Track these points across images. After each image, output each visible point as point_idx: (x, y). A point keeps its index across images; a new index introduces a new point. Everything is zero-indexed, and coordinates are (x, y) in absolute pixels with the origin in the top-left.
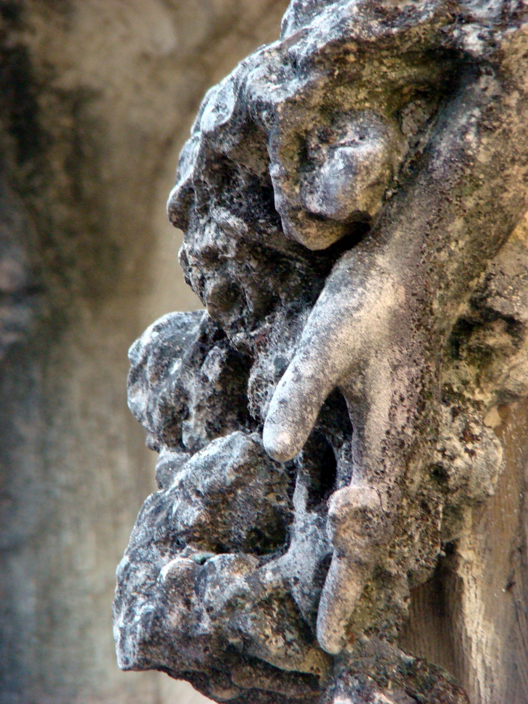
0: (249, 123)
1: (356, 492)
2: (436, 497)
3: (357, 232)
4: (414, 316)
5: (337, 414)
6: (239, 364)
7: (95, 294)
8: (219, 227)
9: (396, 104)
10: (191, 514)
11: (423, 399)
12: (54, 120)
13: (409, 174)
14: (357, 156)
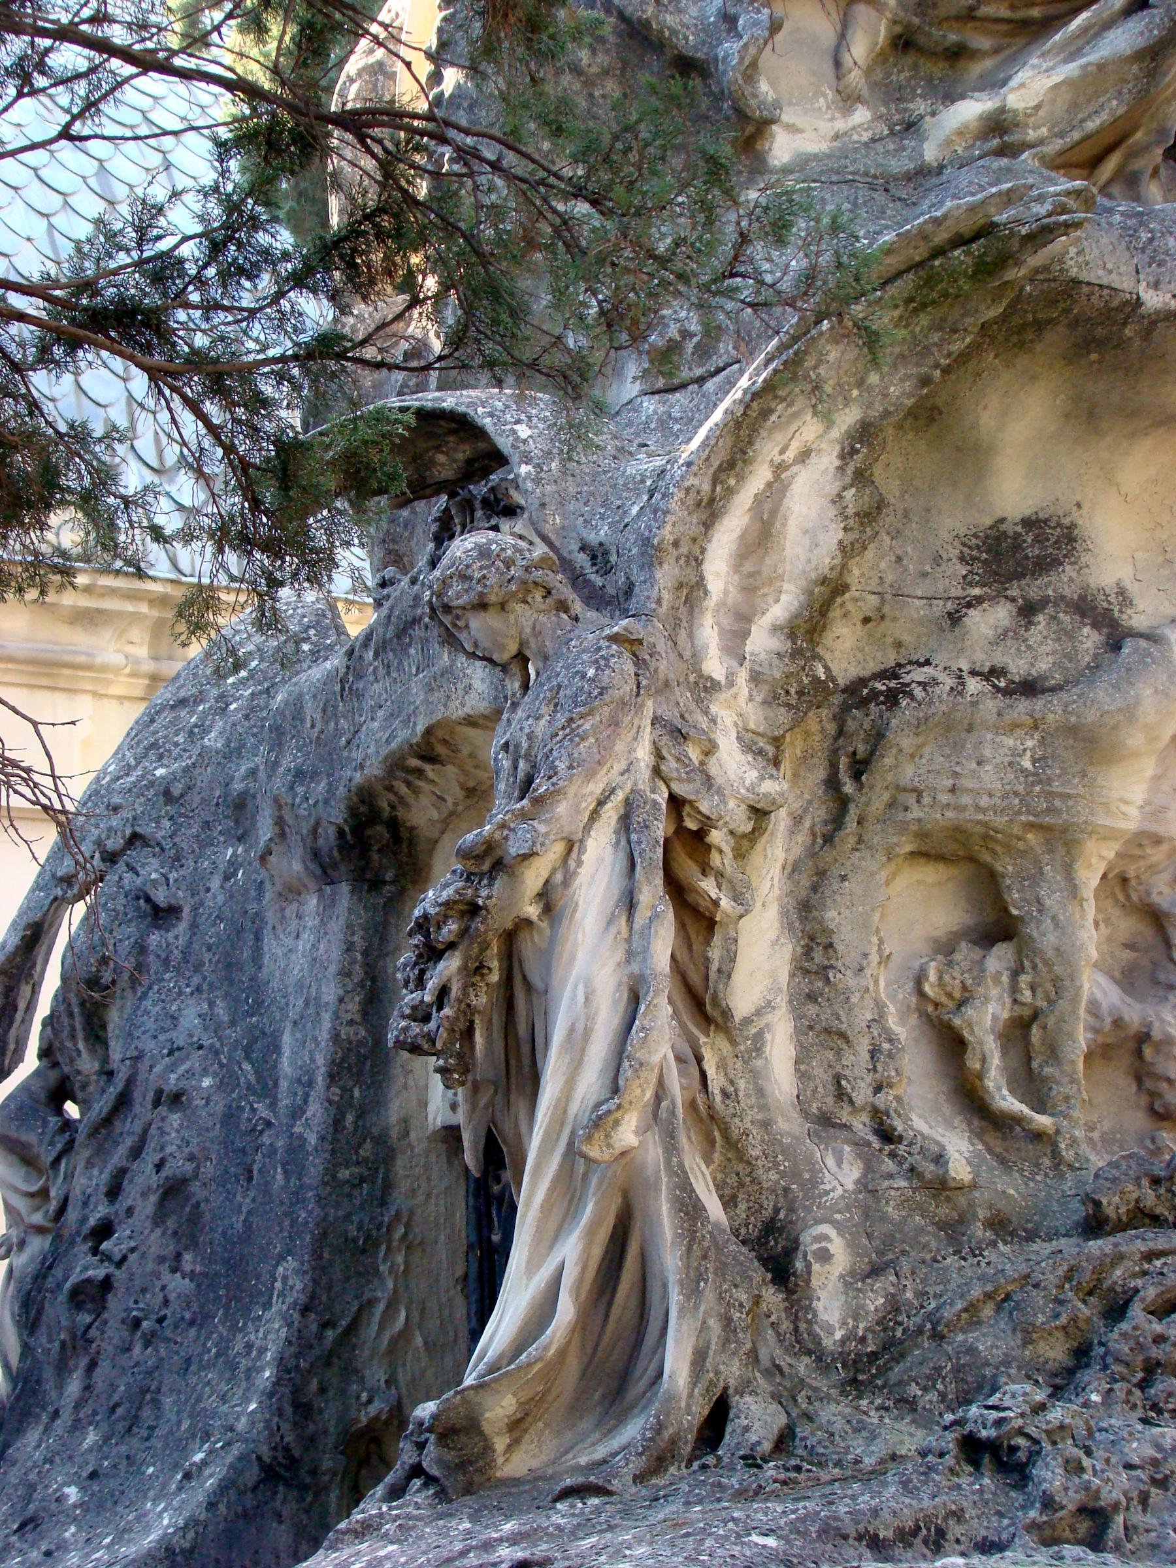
0: (426, 916)
1: (447, 1011)
2: (468, 1011)
3: (451, 946)
4: (464, 968)
5: (443, 993)
6: (422, 972)
7: (414, 882)
8: (417, 939)
9: (462, 914)
10: (408, 1011)
11: (465, 989)
12: (404, 834)
13: (464, 932)
14: (451, 928)
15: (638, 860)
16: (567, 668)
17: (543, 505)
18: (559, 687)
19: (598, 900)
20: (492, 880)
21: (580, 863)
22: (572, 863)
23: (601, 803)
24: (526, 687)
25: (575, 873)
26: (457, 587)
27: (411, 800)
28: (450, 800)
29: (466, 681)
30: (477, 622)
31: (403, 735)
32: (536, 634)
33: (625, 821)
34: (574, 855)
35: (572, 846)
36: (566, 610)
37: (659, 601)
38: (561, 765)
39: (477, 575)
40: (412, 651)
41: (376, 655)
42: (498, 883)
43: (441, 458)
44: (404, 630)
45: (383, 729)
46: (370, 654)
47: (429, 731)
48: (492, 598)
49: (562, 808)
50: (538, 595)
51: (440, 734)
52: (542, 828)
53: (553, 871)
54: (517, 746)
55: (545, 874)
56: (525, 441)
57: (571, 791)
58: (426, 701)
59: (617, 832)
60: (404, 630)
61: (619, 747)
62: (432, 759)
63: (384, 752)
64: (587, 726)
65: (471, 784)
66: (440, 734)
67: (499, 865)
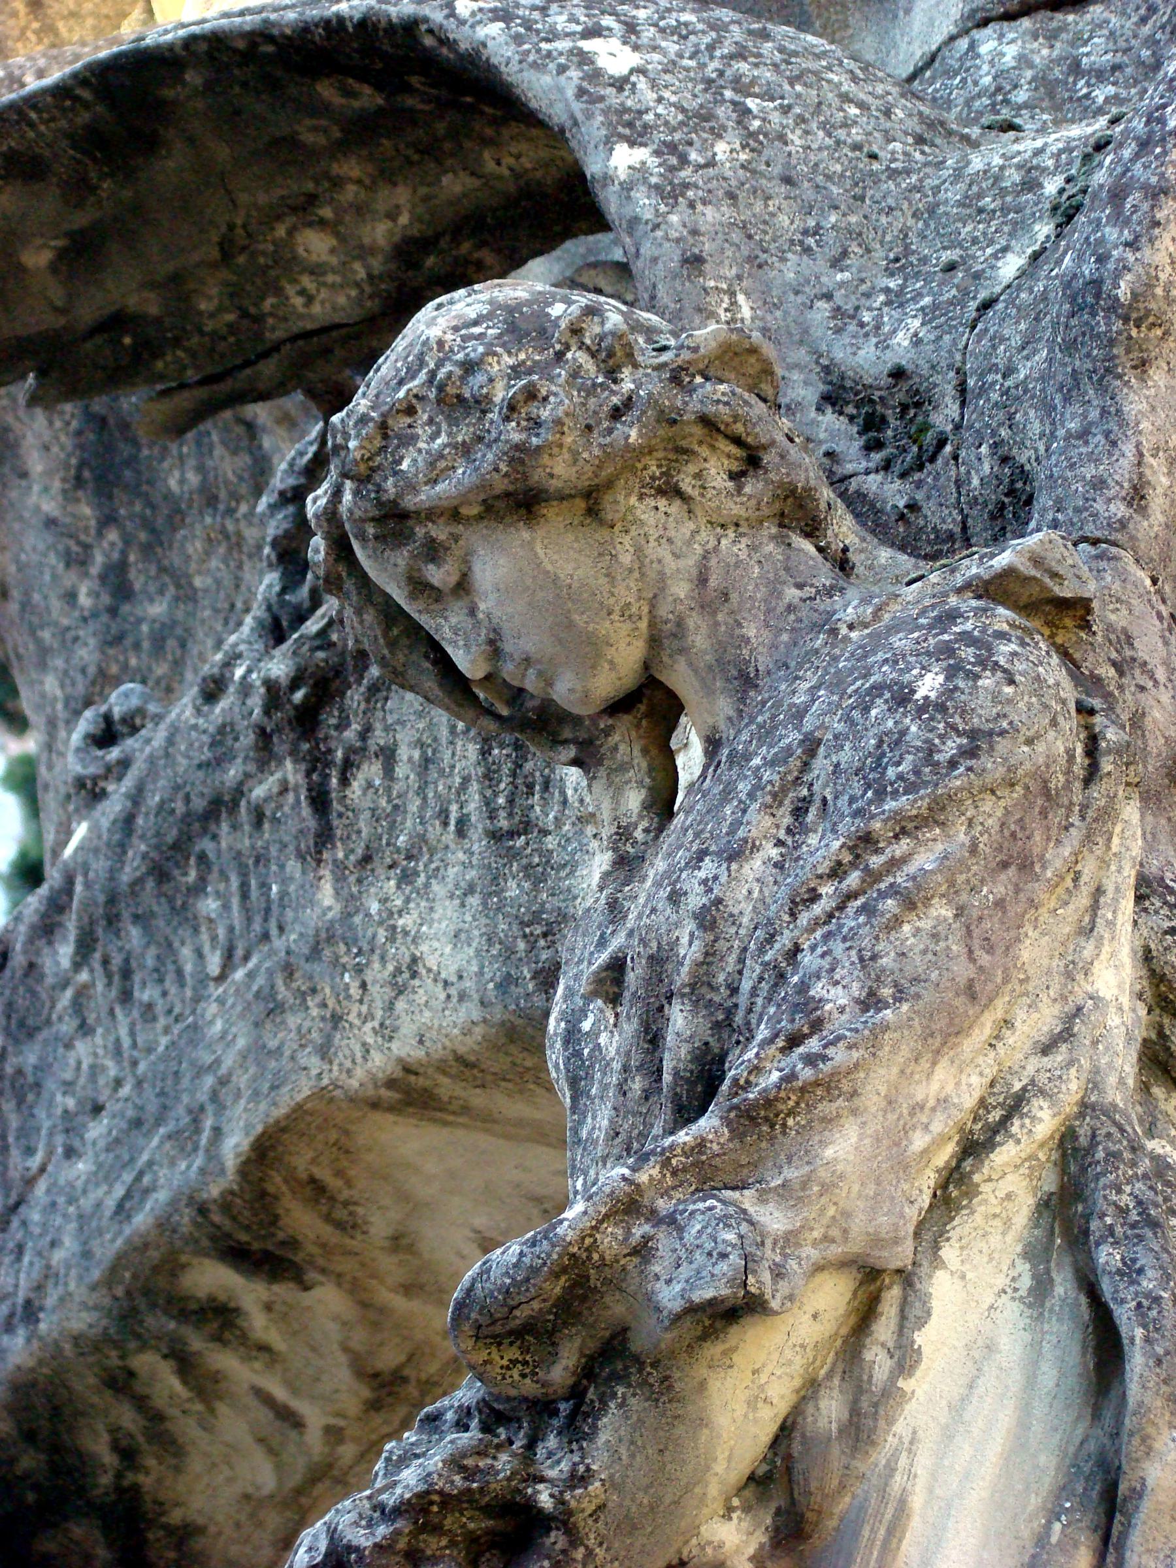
15: (1132, 1331)
16: (838, 685)
17: (694, 262)
18: (811, 746)
19: (977, 1495)
20: (577, 1430)
21: (906, 1358)
22: (878, 1359)
23: (974, 1148)
24: (662, 804)
25: (890, 1395)
26: (430, 440)
27: (187, 1428)
28: (315, 1417)
29: (400, 952)
30: (500, 566)
31: (173, 1178)
32: (712, 596)
33: (1067, 1214)
34: (884, 1329)
35: (879, 1288)
36: (813, 529)
37: (1137, 496)
38: (836, 997)
39: (500, 394)
40: (209, 905)
41: (85, 946)
42: (609, 1428)
43: (316, 245)
44: (180, 848)
45: (104, 1175)
46: (65, 952)
47: (265, 1151)
48: (560, 470)
49: (843, 1147)
50: (716, 468)
51: (302, 1160)
52: (774, 1219)
53: (810, 1389)
54: (659, 961)
55: (780, 1395)
56: (620, 84)
57: (877, 1083)
58: (259, 1052)
59: (1036, 1254)
60: (180, 848)
61: (1035, 951)
62: (271, 1260)
63: (108, 1247)
64: (925, 860)
65: (389, 1359)
66: (302, 1160)
67: (614, 1361)
